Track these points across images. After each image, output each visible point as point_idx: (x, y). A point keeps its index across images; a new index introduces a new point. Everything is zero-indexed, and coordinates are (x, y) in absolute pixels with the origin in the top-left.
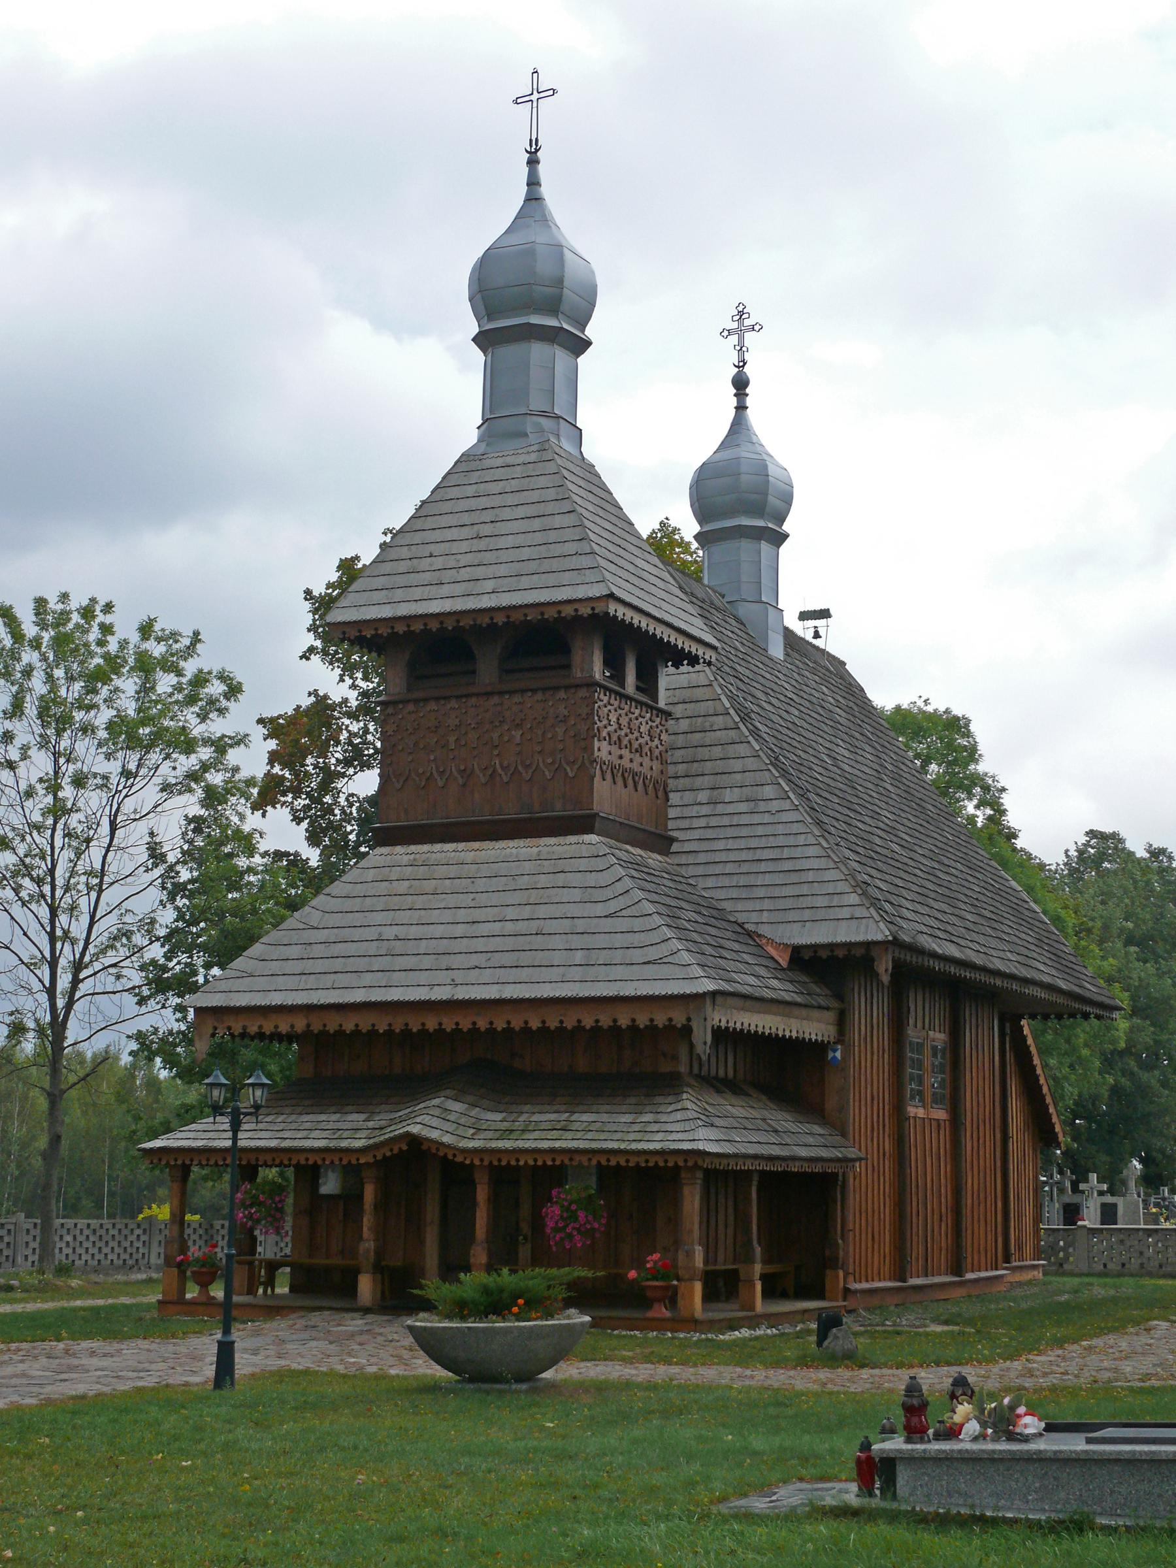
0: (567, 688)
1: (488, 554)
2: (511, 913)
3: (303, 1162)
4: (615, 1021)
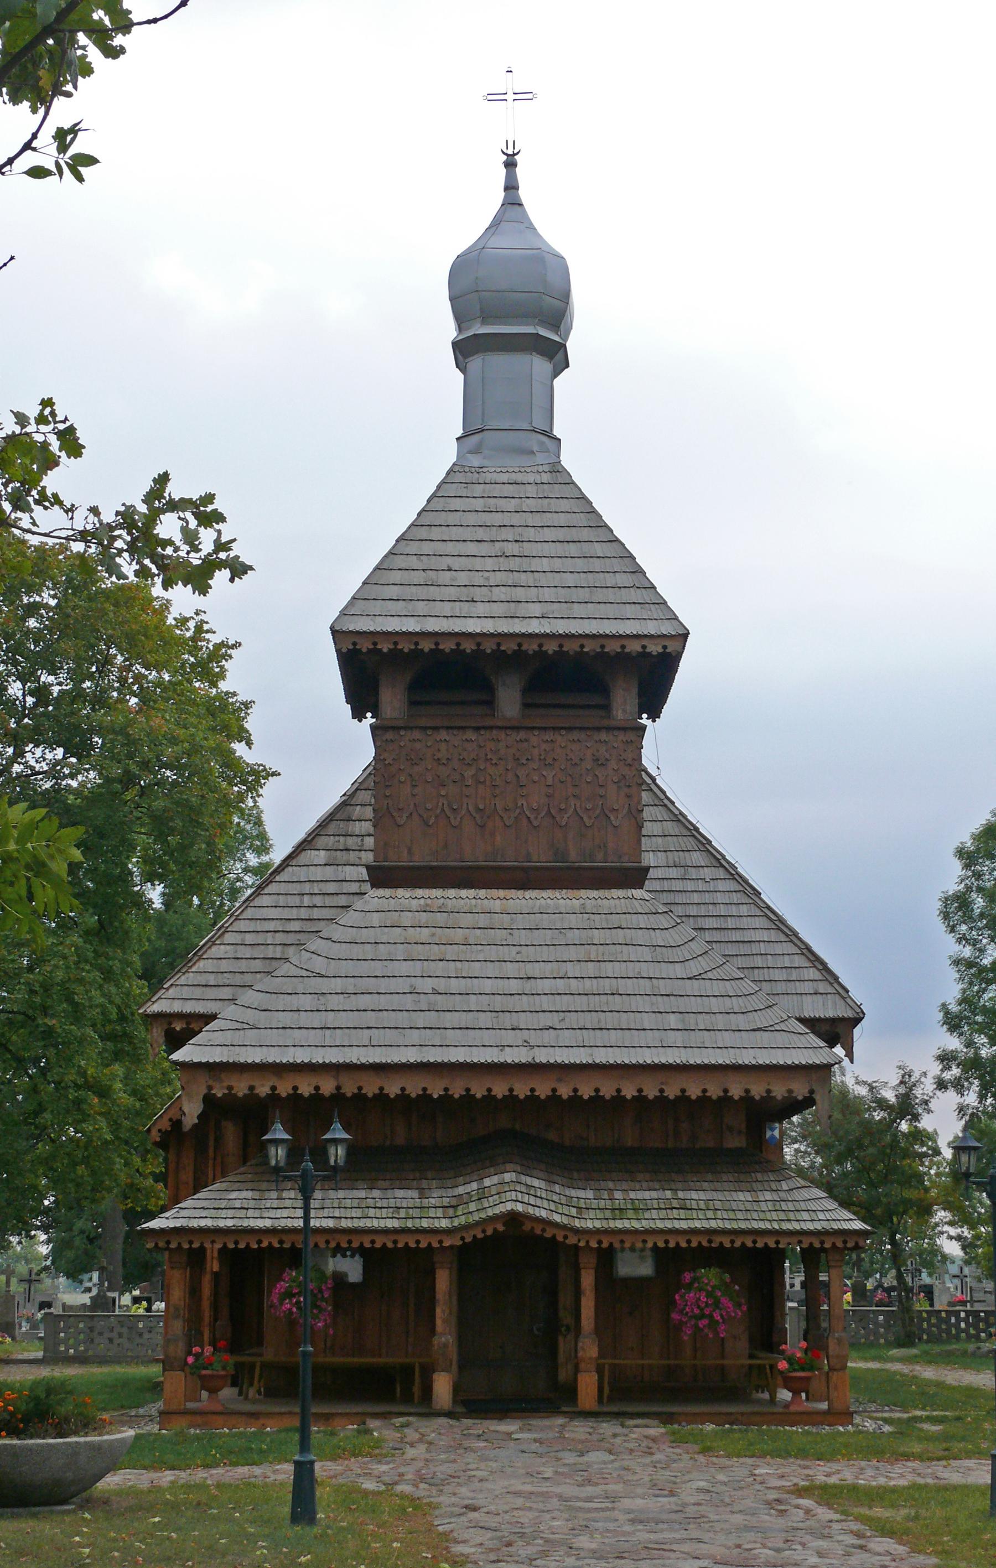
0: (609, 729)
1: (523, 576)
2: (572, 970)
3: (368, 1245)
4: (726, 1091)
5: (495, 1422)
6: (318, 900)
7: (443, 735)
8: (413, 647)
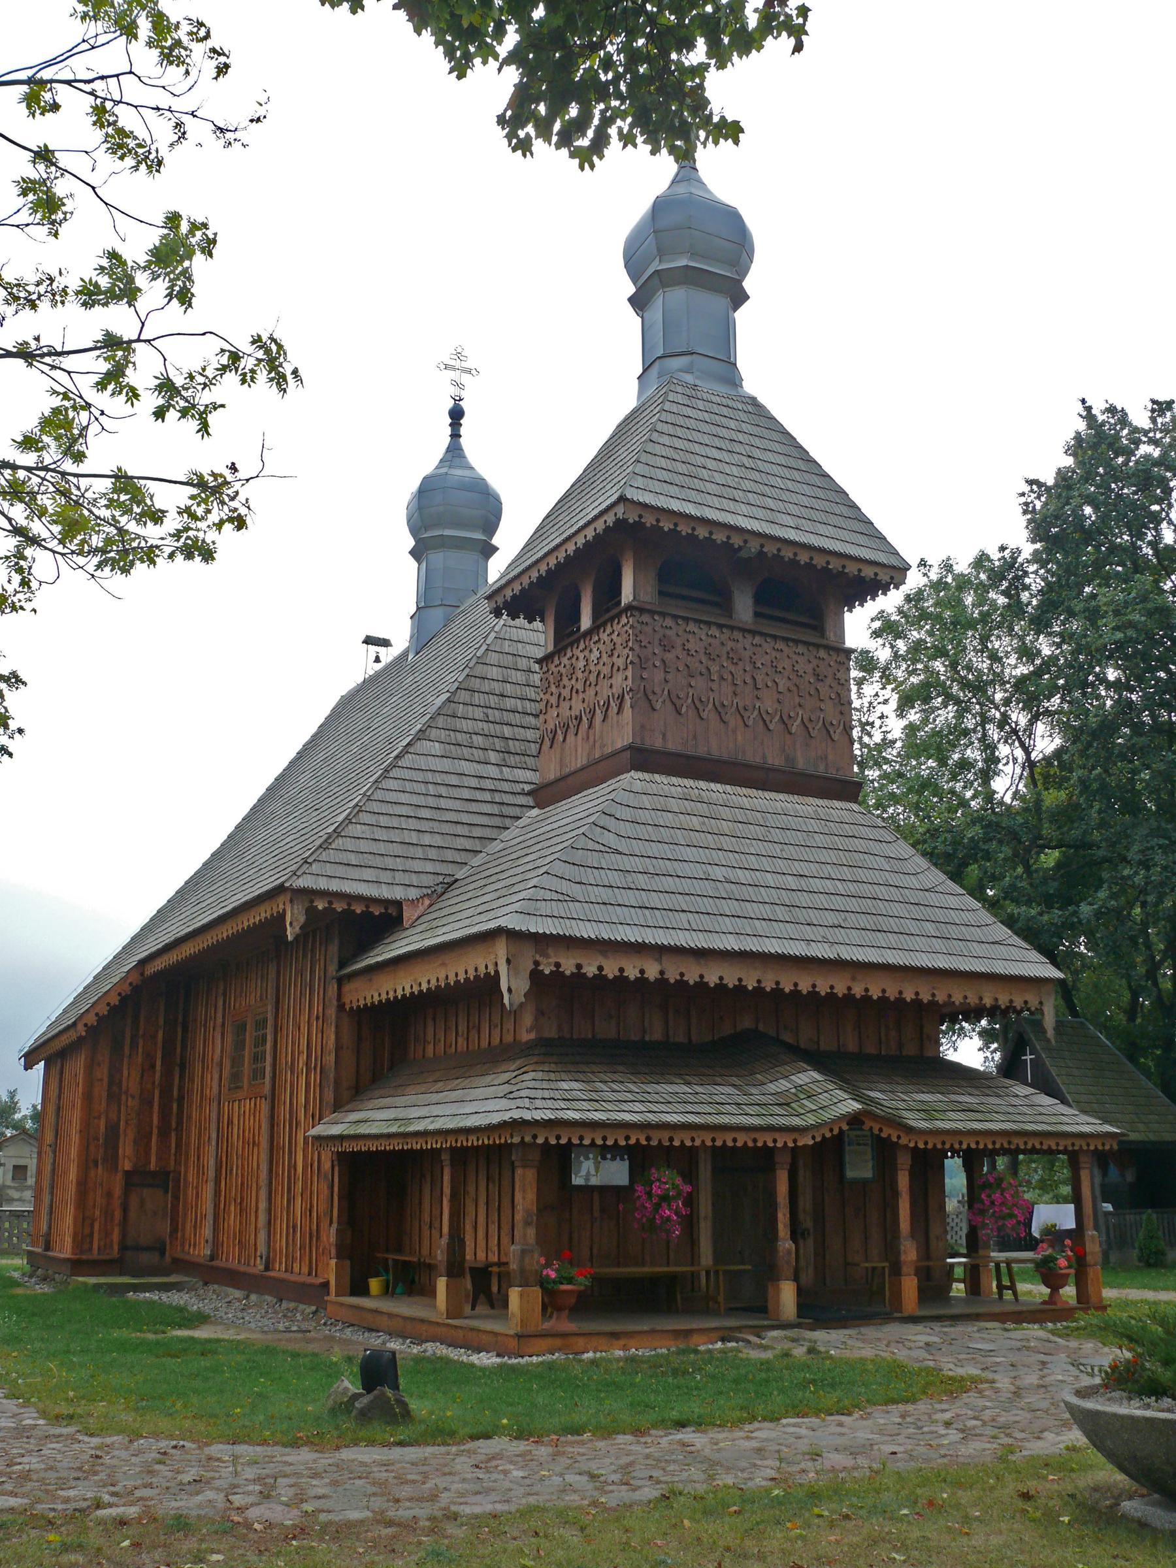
5: (872, 1328)
6: (443, 791)
7: (692, 627)
8: (690, 531)
